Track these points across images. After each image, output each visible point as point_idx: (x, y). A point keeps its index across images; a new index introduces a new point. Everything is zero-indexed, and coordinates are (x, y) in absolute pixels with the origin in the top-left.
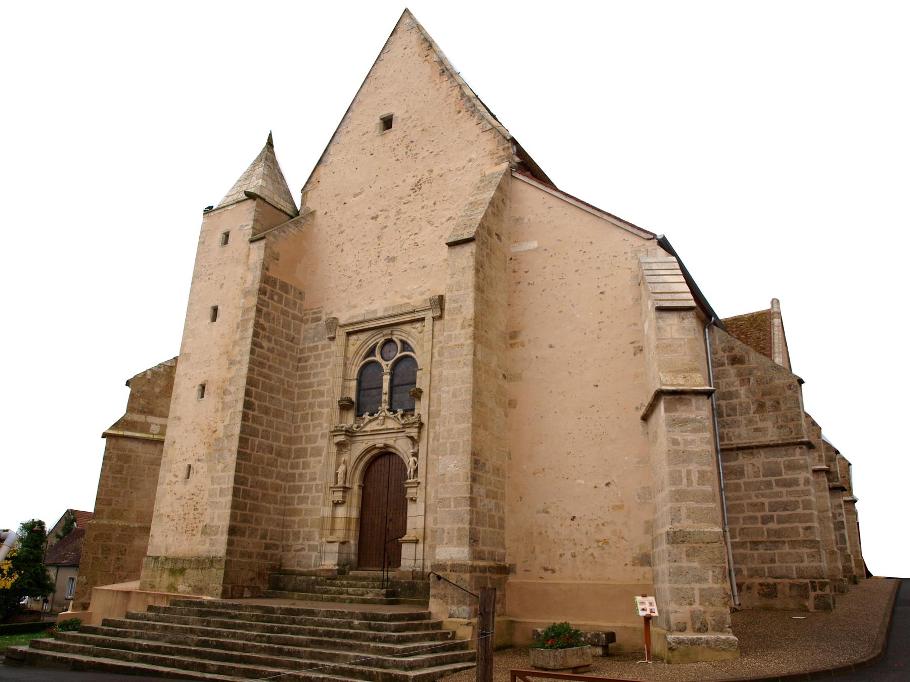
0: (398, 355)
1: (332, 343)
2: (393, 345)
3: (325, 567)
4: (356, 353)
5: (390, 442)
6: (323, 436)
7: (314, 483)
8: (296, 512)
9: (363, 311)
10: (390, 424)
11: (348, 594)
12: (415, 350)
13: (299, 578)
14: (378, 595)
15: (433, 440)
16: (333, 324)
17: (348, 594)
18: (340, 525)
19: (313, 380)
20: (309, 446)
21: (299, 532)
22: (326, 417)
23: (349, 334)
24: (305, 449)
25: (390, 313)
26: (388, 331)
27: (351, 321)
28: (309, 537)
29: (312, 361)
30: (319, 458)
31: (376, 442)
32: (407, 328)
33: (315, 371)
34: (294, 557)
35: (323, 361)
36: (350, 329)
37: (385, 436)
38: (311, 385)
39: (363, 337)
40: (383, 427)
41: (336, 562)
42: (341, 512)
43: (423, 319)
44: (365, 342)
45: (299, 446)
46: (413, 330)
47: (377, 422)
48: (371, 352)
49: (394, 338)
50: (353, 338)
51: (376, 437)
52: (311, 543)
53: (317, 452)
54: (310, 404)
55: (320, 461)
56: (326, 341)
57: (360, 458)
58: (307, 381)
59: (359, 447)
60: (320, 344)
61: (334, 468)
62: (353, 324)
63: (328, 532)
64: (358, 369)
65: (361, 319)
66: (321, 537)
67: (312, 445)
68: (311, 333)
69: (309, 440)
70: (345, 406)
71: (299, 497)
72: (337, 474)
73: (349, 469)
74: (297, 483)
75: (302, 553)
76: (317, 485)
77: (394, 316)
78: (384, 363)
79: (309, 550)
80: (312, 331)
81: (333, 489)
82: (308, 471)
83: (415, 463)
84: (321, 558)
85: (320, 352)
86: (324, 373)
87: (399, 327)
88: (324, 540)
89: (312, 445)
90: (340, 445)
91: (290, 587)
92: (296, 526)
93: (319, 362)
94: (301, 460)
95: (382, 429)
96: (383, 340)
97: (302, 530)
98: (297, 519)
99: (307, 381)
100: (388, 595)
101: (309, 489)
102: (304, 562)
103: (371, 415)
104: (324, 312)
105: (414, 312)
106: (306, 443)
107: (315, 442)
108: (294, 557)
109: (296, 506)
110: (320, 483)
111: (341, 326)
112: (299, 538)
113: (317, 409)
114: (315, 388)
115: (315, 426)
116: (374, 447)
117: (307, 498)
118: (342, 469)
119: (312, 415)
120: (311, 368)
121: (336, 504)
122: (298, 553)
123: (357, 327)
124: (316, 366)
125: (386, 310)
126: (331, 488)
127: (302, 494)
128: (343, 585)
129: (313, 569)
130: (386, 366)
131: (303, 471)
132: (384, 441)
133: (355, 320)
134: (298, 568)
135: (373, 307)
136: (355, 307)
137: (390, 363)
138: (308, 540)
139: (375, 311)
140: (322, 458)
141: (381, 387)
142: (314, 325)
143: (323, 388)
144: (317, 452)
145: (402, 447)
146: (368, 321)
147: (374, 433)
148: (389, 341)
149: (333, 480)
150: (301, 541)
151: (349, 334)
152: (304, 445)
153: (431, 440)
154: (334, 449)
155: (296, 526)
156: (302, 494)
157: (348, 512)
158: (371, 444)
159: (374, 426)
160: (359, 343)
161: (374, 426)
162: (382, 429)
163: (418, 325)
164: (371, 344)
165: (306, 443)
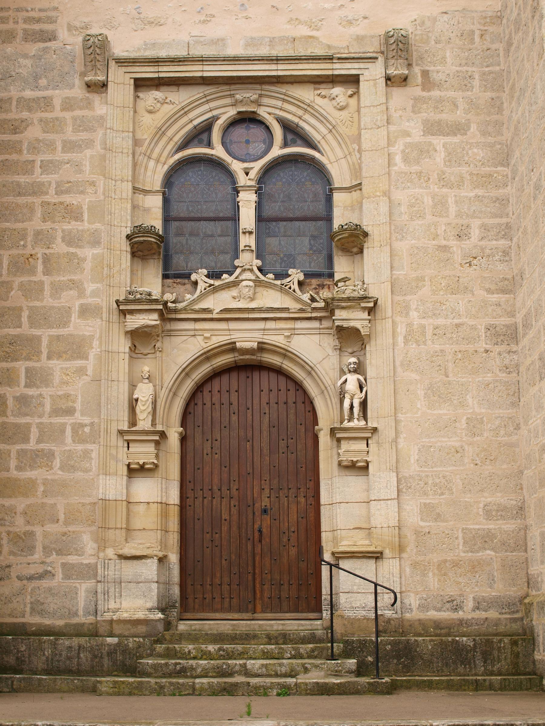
0: (276, 152)
1: (96, 98)
2: (256, 131)
3: (125, 615)
4: (160, 132)
5: (277, 340)
6: (85, 311)
7: (68, 420)
8: (26, 488)
9: (185, 38)
10: (271, 299)
11: (247, 673)
12: (323, 145)
13: (65, 642)
14: (337, 674)
15: (406, 341)
16: (97, 50)
17: (247, 673)
18: (146, 519)
19: (39, 176)
20: (45, 334)
21: (31, 534)
22: (96, 273)
23: (140, 84)
24: (33, 342)
25: (264, 51)
26: (250, 94)
27: (149, 54)
28: (63, 546)
29: (34, 132)
30: (79, 363)
31: (235, 336)
32: (305, 93)
33: (47, 157)
34: (21, 592)
35: (69, 134)
36: (148, 72)
37: (261, 325)
38: (37, 190)
39: (181, 97)
40: (253, 305)
41: (152, 602)
42: (146, 490)
43: (353, 80)
44: (184, 111)
45: (13, 331)
46: (319, 101)
47: (234, 292)
48: (201, 133)
49: (263, 113)
50: (151, 97)
51: (233, 325)
52: (72, 559)
53: (76, 348)
54: (38, 233)
55: (81, 371)
56: (78, 91)
57: (186, 372)
58: (22, 179)
59: (186, 347)
60: (58, 95)
61: (125, 387)
62: (156, 61)
63: (120, 535)
64: (162, 170)
65: (182, 53)
66: (102, 544)
67: (54, 332)
68: (26, 66)
69: (40, 318)
70: (143, 246)
71: (21, 453)
72: (133, 404)
73: (163, 394)
74: (11, 419)
75: (45, 583)
76: (77, 428)
77: (277, 60)
78: (236, 166)
79: (67, 577)
80: (28, 62)
81: (129, 436)
82: (45, 391)
83: (361, 388)
84: (106, 593)
85: (57, 113)
86: (78, 167)
87: (283, 89)
88: (110, 552)
89: (54, 332)
90: (140, 338)
91: (39, 663)
92: (20, 521)
93: (57, 139)
94: (21, 366)
95: (246, 307)
96: (232, 112)
97: (38, 530)
98: (20, 503)
99: (22, 179)
100: (360, 670)
101: (50, 433)
102: (52, 604)
103: (214, 275)
104: (63, 21)
105: (330, 59)
106: (33, 324)
107: (65, 324)
108: (21, 592)
109: (14, 473)
110: (86, 420)
111: (121, 62)
112: (31, 549)
113: (60, 247)
114: (51, 197)
115: (57, 289)
116: (231, 348)
117: (51, 455)
118: (144, 392)
119: (47, 259)
120: (34, 149)
121: (135, 471)
122: (35, 583)
123: (167, 71)
124: (51, 146)
125: (251, 42)
126: (121, 433)
127: (32, 445)
128: (186, 656)
129: (83, 619)
130: (246, 173)
131: (31, 392)
132: (258, 336)
133: (163, 54)
134: (36, 620)
135: (214, 31)
136: (156, 23)
137: (257, 166)
138: (60, 552)
139: (221, 41)
140: (90, 364)
141: (235, 218)
142: (34, 48)
143: (84, 201)
144: (76, 348)
145: (312, 349)
146: (202, 60)
147: (229, 316)
148: (248, 119)
149: (125, 415)
150: (38, 556)
151: (140, 84)
152: (26, 329)
153: (400, 340)
154: (123, 345)
155: (20, 521)
156: (32, 445)
157: (159, 492)
158: (217, 340)
159: (217, 303)
160: (167, 110)
161: (217, 303)
162: (246, 307)
163: (339, 92)
164: (198, 117)
165: (33, 324)
